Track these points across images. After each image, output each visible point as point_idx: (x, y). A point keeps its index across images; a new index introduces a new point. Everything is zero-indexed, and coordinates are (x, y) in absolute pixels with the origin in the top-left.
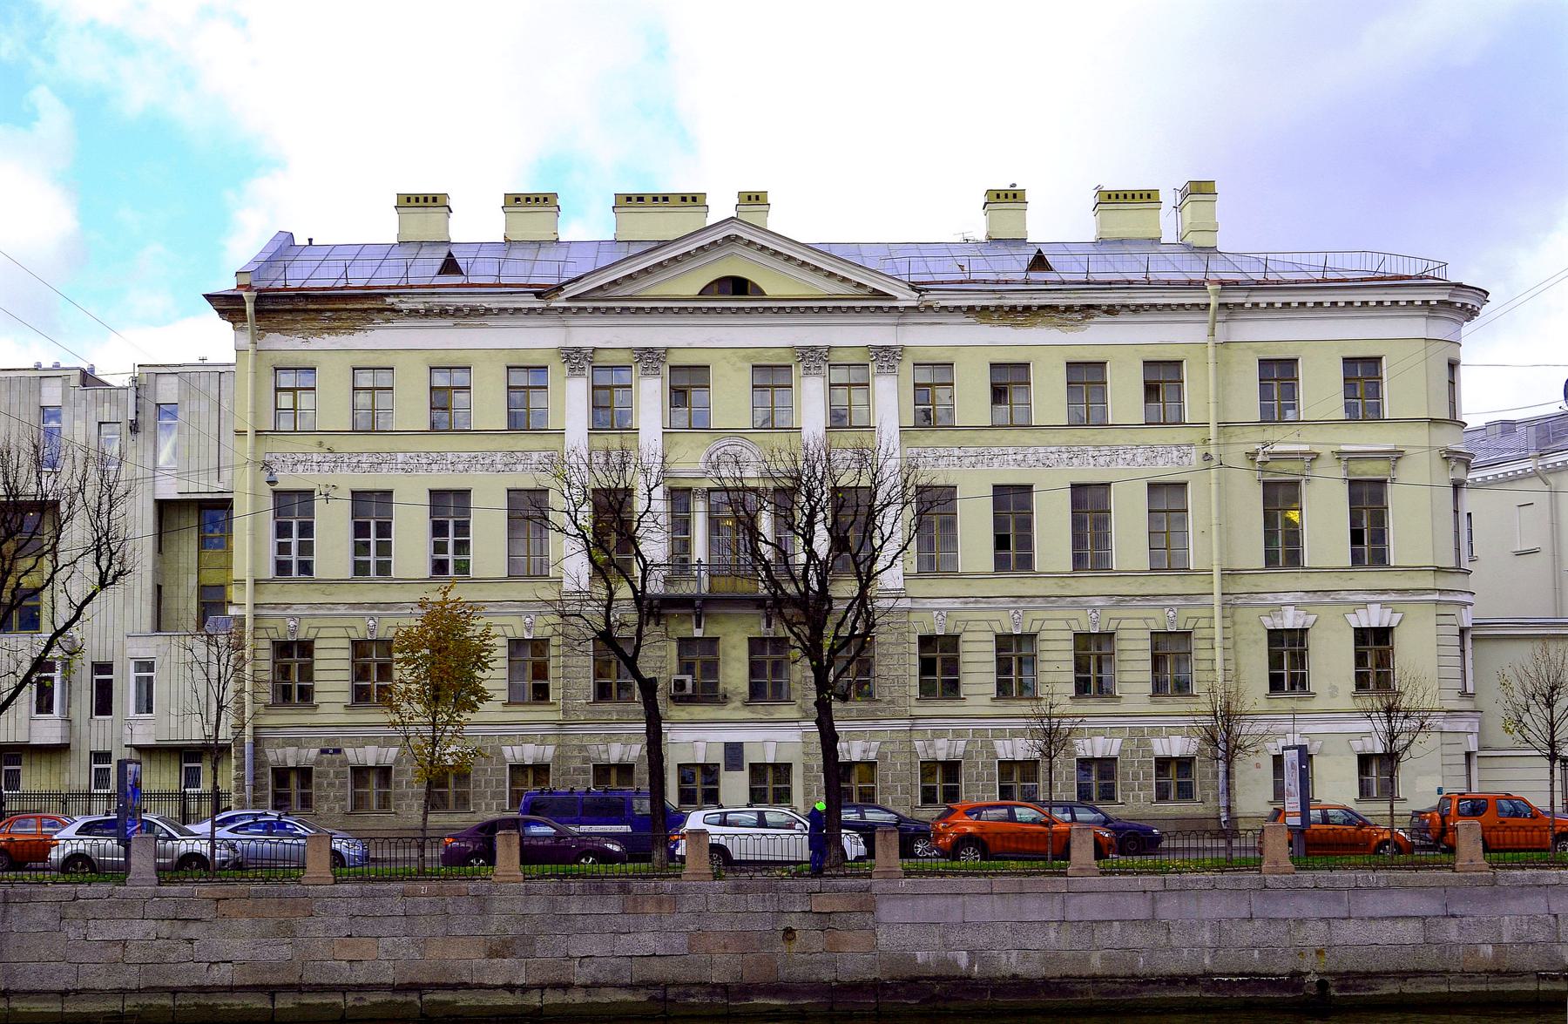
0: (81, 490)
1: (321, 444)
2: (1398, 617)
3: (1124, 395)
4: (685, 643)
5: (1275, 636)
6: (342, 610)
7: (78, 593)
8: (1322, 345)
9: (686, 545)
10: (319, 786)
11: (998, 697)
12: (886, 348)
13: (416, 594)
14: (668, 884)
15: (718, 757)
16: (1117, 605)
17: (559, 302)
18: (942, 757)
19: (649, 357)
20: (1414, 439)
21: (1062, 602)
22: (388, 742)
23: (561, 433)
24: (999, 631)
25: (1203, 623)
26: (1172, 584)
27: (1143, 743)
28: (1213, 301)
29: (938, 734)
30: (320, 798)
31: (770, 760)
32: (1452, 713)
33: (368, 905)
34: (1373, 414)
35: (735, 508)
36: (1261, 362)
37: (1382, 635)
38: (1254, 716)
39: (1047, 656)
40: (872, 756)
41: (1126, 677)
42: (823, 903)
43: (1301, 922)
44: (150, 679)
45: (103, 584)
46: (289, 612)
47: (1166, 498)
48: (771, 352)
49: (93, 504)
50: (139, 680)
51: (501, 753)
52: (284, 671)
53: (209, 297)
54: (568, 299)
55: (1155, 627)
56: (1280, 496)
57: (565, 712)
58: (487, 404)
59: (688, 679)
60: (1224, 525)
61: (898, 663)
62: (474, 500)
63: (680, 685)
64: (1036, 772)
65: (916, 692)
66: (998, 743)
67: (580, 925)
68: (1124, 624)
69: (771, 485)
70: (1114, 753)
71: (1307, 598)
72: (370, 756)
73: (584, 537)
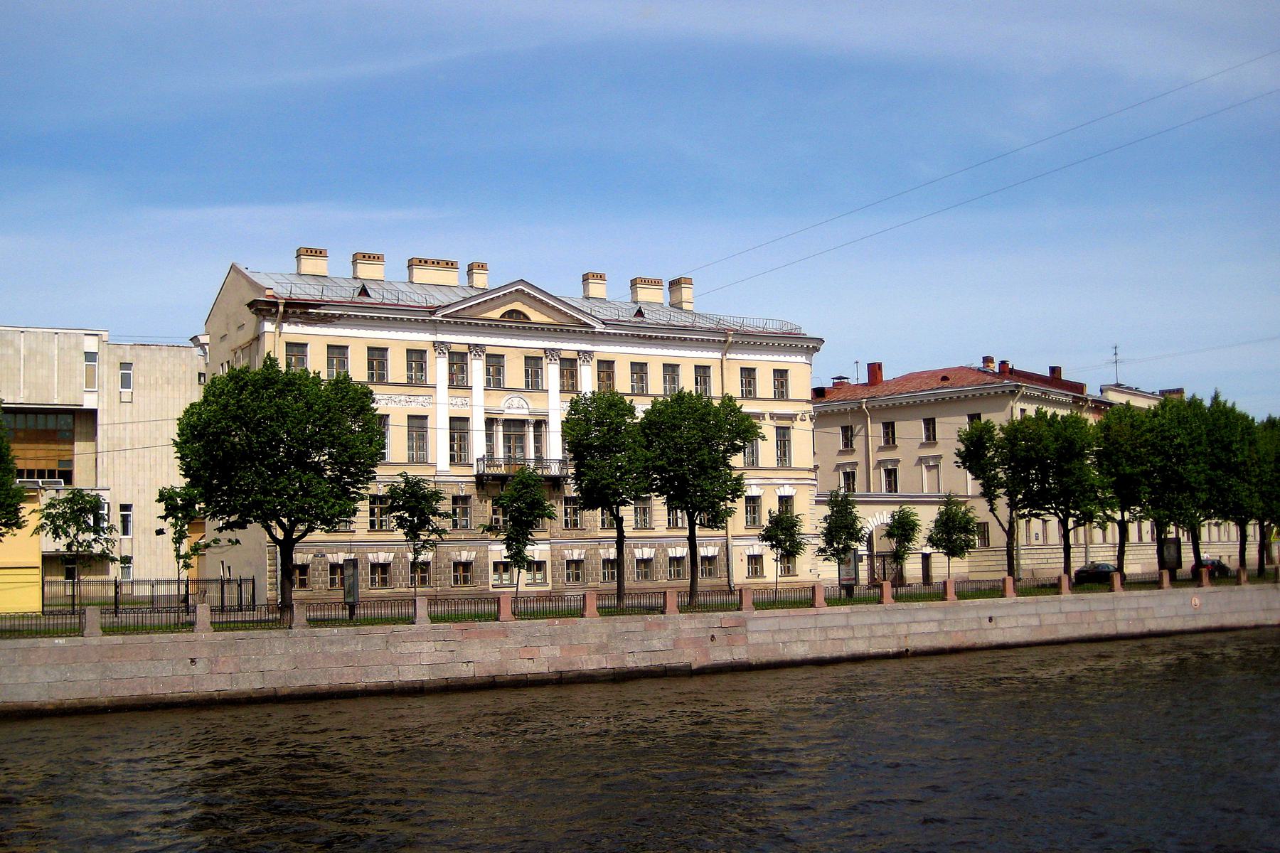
8: (765, 364)
13: (400, 470)
17: (438, 317)
27: (665, 550)
35: (515, 427)
65: (600, 524)
66: (636, 551)
69: (534, 418)
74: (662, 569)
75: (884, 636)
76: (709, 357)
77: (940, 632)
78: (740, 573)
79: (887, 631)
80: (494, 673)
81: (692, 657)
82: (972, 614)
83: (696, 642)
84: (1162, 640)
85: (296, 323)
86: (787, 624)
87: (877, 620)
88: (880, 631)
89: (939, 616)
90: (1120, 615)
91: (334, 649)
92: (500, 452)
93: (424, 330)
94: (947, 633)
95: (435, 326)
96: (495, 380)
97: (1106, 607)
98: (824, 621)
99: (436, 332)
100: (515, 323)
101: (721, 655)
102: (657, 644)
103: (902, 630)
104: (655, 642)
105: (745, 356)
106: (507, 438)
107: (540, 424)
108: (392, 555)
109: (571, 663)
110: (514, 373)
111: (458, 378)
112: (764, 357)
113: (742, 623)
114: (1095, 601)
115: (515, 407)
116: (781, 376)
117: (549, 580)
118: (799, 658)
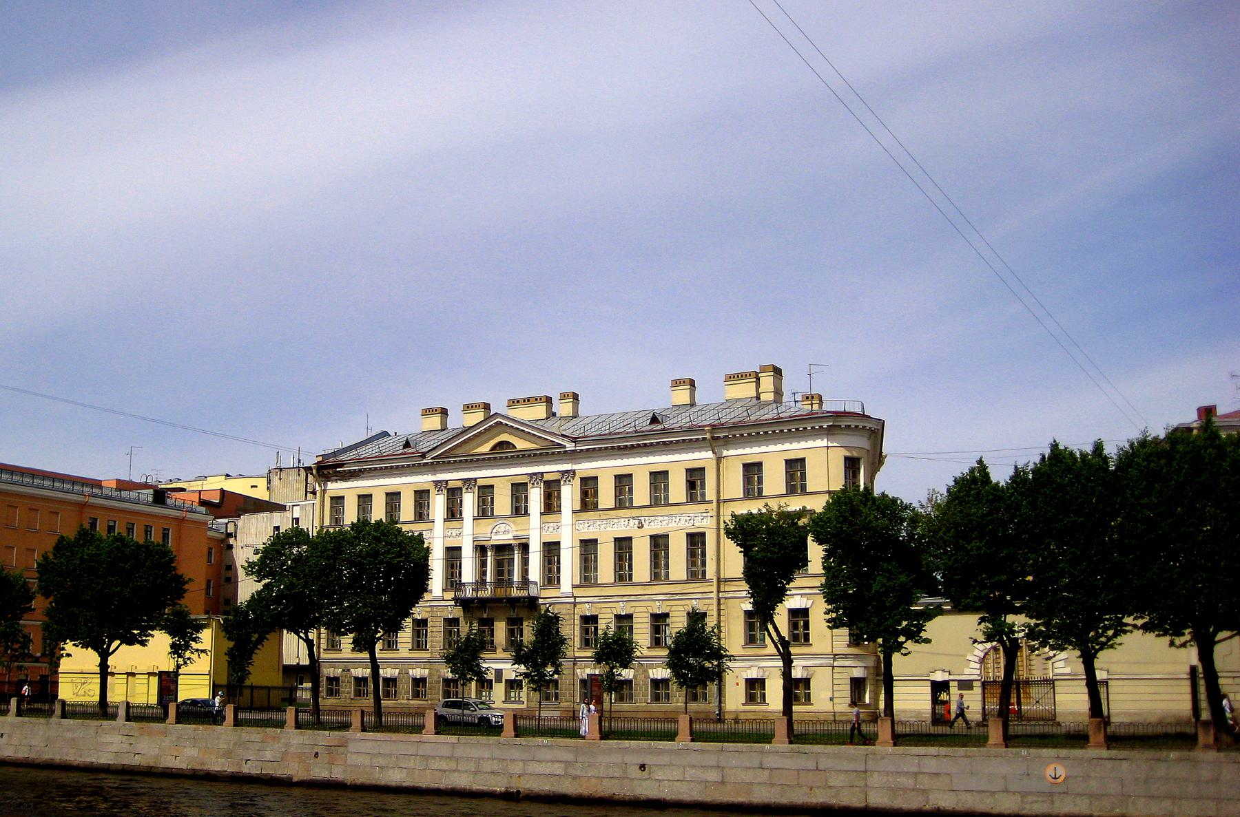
3: (677, 488)
9: (484, 573)
11: (746, 644)
27: (646, 671)
28: (708, 436)
32: (845, 656)
36: (744, 465)
38: (731, 658)
52: (586, 631)
68: (638, 610)
74: (347, 689)
75: (492, 773)
76: (702, 457)
77: (566, 775)
78: (735, 698)
79: (496, 767)
80: (152, 764)
81: (295, 770)
82: (616, 758)
83: (301, 757)
84: (323, 793)
85: (336, 481)
86: (387, 748)
87: (487, 754)
88: (487, 766)
89: (569, 757)
90: (875, 780)
91: (69, 735)
92: (489, 578)
93: (427, 473)
94: (575, 778)
95: (432, 467)
96: (485, 510)
97: (851, 767)
98: (426, 750)
99: (435, 472)
100: (504, 454)
101: (320, 772)
102: (268, 755)
103: (517, 768)
105: (748, 450)
106: (499, 564)
107: (525, 548)
109: (203, 764)
110: (503, 502)
112: (772, 448)
113: (343, 744)
114: (738, 757)
115: (504, 533)
116: (795, 467)
117: (524, 699)
118: (394, 784)
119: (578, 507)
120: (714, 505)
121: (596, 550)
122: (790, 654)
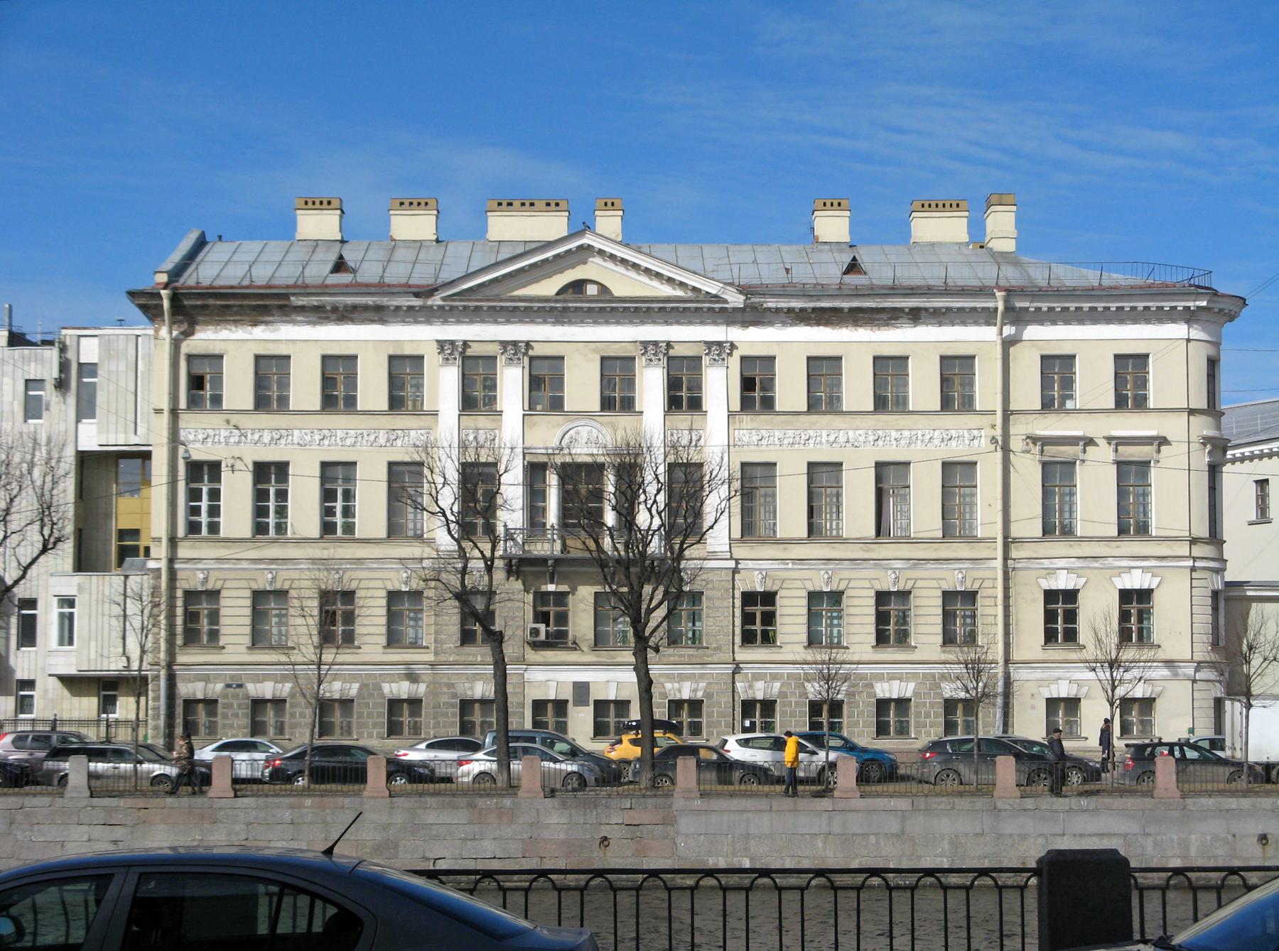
0: (30, 472)
1: (228, 422)
2: (1157, 580)
4: (541, 597)
5: (1050, 596)
6: (245, 565)
7: (26, 554)
10: (293, 715)
12: (719, 344)
14: (507, 802)
15: (567, 694)
16: (914, 567)
17: (436, 301)
18: (760, 696)
19: (515, 349)
20: (1175, 427)
21: (865, 564)
22: (284, 679)
23: (435, 414)
24: (812, 589)
25: (987, 584)
26: (962, 550)
29: (757, 677)
30: (224, 726)
31: (612, 697)
33: (262, 814)
34: (1141, 403)
35: (579, 479)
36: (1043, 358)
37: (1144, 595)
39: (852, 611)
40: (699, 695)
41: (921, 629)
42: (636, 817)
43: (1023, 837)
44: (71, 615)
45: (44, 550)
46: (200, 566)
47: (957, 474)
48: (618, 346)
49: (38, 483)
50: (62, 615)
51: (380, 689)
53: (132, 294)
54: (444, 299)
55: (947, 587)
56: (1058, 476)
57: (436, 654)
58: (372, 387)
59: (542, 627)
60: (1007, 497)
61: (720, 618)
62: (360, 472)
63: (535, 632)
64: (773, 710)
67: (434, 833)
70: (908, 695)
71: (1079, 563)
72: (267, 690)
73: (444, 515)
92: (552, 517)
104: (486, 843)
106: (566, 497)
108: (912, 686)
110: (582, 386)
111: (477, 396)
115: (589, 439)
119: (736, 406)
120: (998, 419)
121: (839, 480)
122: (907, 681)
